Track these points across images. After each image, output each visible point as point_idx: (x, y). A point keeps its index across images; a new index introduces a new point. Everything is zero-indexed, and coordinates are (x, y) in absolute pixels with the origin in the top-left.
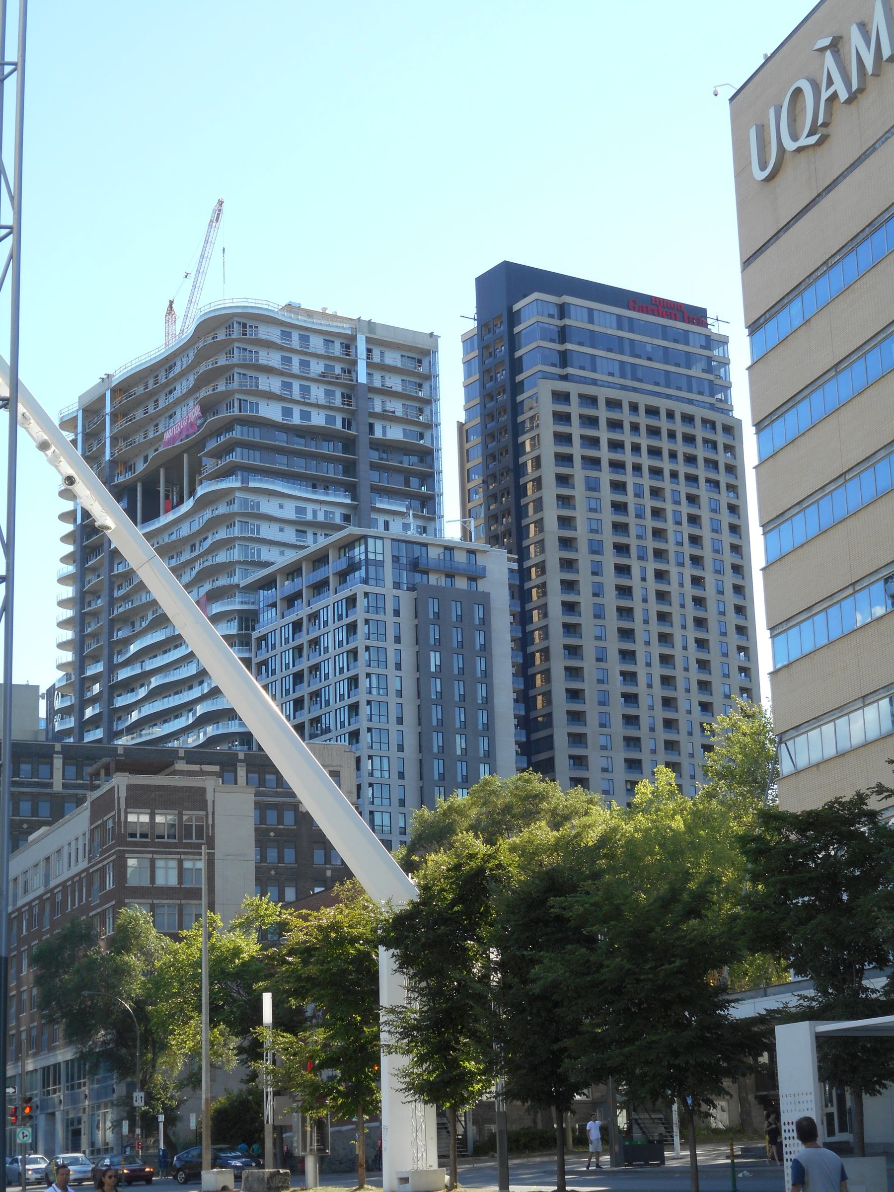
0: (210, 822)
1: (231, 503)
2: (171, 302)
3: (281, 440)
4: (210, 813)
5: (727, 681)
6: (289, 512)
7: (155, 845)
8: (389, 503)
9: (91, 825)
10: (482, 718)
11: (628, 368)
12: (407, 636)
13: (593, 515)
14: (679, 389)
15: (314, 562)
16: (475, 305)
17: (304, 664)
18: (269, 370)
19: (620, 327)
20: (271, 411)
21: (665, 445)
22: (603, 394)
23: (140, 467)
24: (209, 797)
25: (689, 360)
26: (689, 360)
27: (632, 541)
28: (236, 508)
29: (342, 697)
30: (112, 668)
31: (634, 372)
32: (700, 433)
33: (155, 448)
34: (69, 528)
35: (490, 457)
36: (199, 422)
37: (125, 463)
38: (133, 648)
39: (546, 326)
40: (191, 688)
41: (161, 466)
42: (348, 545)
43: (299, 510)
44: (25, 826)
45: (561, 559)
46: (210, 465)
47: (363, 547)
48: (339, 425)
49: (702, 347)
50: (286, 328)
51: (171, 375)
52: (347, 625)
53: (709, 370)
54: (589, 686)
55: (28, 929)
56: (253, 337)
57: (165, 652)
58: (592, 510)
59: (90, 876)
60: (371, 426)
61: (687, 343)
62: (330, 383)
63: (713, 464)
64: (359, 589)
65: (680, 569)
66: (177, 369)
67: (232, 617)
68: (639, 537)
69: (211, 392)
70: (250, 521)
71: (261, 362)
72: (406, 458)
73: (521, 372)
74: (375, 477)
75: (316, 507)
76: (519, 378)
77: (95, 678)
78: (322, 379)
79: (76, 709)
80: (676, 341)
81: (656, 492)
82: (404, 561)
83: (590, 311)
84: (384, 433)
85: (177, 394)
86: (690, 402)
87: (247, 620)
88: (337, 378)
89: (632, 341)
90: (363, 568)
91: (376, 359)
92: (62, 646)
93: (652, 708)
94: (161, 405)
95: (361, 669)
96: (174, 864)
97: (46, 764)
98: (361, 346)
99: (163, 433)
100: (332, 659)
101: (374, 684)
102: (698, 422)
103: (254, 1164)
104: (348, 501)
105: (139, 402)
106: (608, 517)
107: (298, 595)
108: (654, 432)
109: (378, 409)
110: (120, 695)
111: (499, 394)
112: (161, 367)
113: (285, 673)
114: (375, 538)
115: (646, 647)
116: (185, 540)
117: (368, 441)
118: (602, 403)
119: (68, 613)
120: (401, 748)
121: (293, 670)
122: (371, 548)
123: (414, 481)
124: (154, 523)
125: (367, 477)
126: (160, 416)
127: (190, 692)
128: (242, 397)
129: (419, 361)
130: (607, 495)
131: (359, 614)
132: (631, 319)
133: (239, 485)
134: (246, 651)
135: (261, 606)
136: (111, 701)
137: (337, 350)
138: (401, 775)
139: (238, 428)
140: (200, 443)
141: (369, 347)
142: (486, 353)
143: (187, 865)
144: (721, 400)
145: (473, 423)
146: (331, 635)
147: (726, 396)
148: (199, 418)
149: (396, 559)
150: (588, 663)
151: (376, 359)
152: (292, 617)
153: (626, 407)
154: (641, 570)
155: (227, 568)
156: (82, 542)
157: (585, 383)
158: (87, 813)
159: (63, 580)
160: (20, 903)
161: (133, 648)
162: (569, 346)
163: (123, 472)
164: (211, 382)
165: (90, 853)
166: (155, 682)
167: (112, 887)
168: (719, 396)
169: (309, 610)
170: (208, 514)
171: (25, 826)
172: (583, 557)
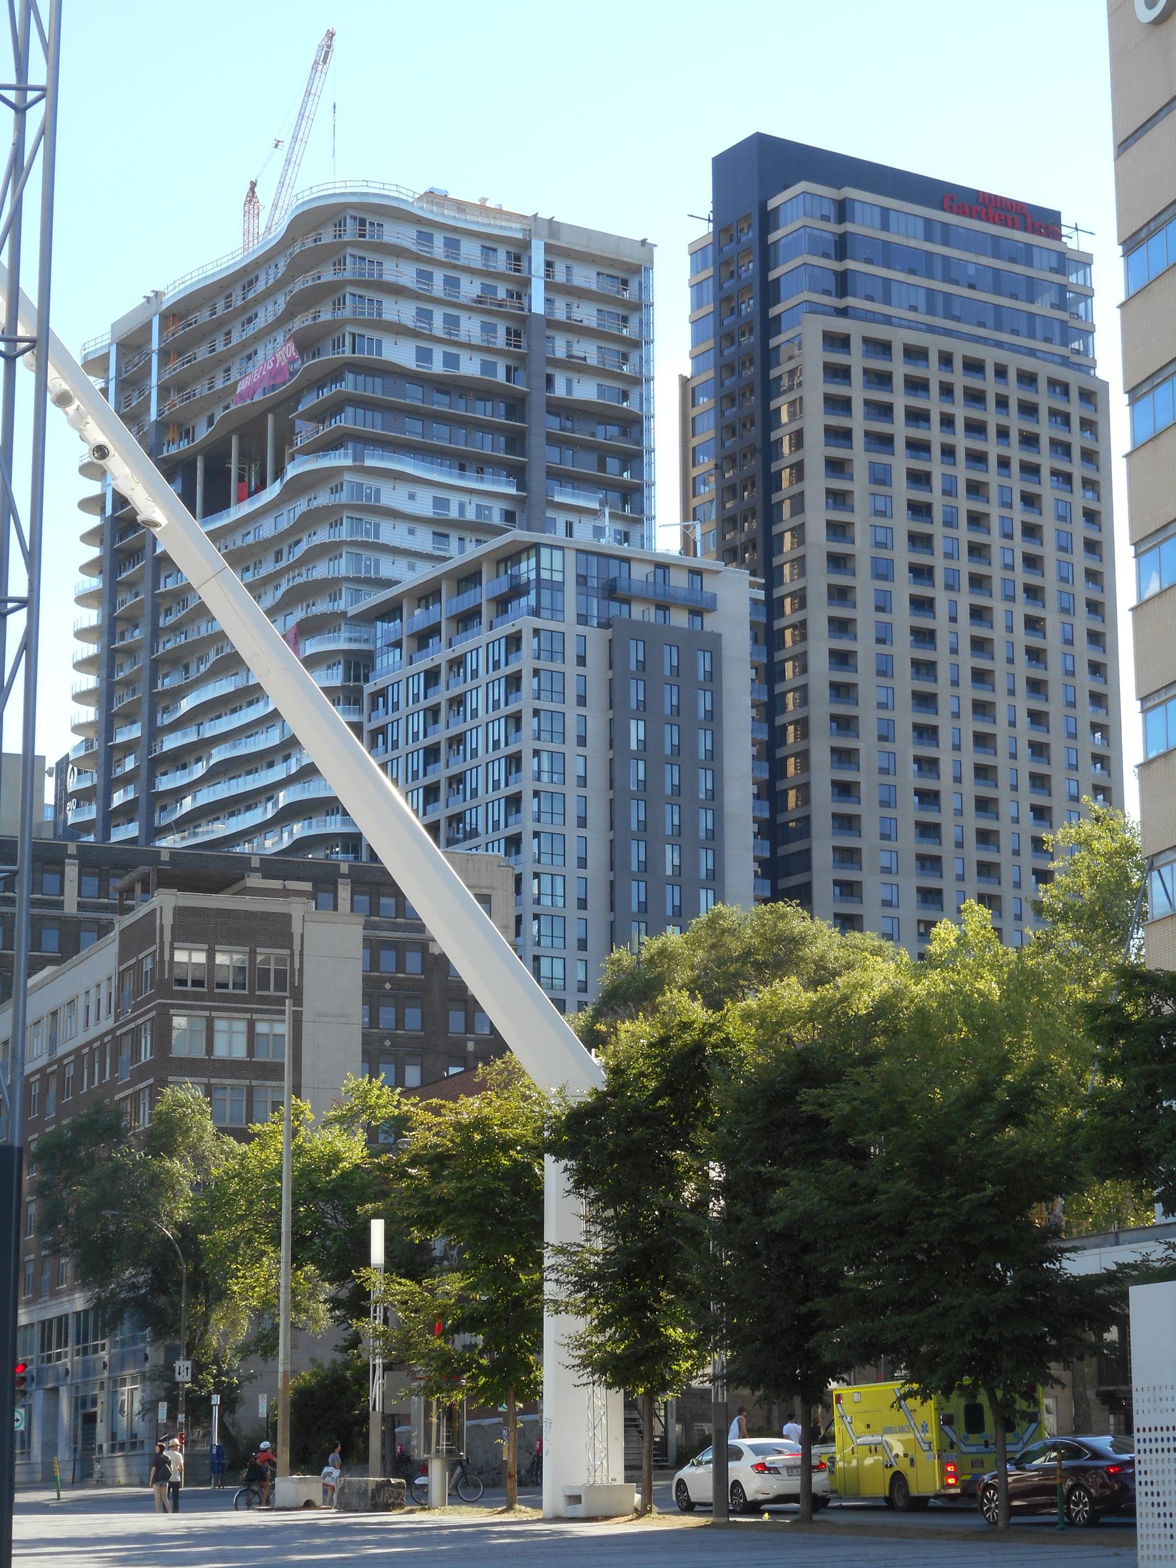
0: (297, 966)
2: (253, 185)
3: (414, 396)
4: (297, 952)
5: (1073, 774)
6: (423, 505)
7: (212, 997)
8: (573, 495)
11: (940, 300)
12: (597, 695)
13: (879, 521)
14: (1015, 332)
15: (459, 582)
16: (710, 198)
17: (441, 734)
18: (397, 291)
19: (928, 238)
21: (991, 417)
22: (900, 338)
23: (202, 433)
24: (296, 929)
25: (1031, 289)
26: (1031, 289)
28: (344, 497)
30: (154, 733)
32: (1044, 400)
35: (727, 429)
37: (180, 426)
38: (186, 705)
40: (271, 765)
43: (440, 503)
45: (830, 586)
46: (306, 433)
48: (501, 377)
49: (1052, 270)
50: (425, 227)
51: (251, 295)
54: (866, 777)
57: (234, 711)
58: (878, 513)
61: (1029, 263)
62: (489, 313)
63: (1062, 448)
65: (1009, 605)
66: (261, 287)
72: (600, 429)
73: (777, 301)
74: (553, 455)
75: (465, 498)
77: (128, 748)
78: (478, 306)
80: (1013, 260)
81: (975, 489)
82: (594, 583)
83: (885, 211)
84: (569, 390)
85: (260, 323)
86: (1032, 353)
87: (357, 665)
88: (500, 306)
89: (946, 259)
90: (533, 592)
91: (560, 277)
93: (959, 812)
94: (236, 339)
95: (525, 743)
96: (241, 1026)
98: (538, 257)
99: (237, 383)
100: (484, 726)
101: (545, 766)
102: (1042, 383)
104: (512, 491)
105: (204, 334)
108: (975, 397)
109: (560, 353)
110: (165, 774)
112: (236, 282)
113: (412, 746)
115: (955, 724)
118: (898, 351)
119: (90, 649)
120: (583, 863)
121: (423, 742)
122: (545, 563)
123: (613, 464)
124: (221, 518)
125: (541, 455)
126: (233, 356)
127: (271, 771)
129: (625, 283)
130: (901, 490)
131: (525, 661)
132: (945, 225)
133: (349, 462)
135: (379, 645)
136: (151, 783)
137: (501, 263)
138: (583, 904)
139: (350, 377)
140: (295, 397)
141: (550, 259)
142: (725, 273)
143: (261, 1028)
144: (1078, 352)
147: (1086, 346)
149: (582, 580)
150: (866, 743)
153: (934, 358)
154: (951, 605)
155: (330, 587)
156: (112, 545)
157: (874, 321)
161: (186, 705)
162: (850, 264)
163: (177, 440)
165: (117, 1006)
166: (219, 754)
167: (149, 1057)
168: (1075, 345)
170: (302, 506)
172: (863, 584)
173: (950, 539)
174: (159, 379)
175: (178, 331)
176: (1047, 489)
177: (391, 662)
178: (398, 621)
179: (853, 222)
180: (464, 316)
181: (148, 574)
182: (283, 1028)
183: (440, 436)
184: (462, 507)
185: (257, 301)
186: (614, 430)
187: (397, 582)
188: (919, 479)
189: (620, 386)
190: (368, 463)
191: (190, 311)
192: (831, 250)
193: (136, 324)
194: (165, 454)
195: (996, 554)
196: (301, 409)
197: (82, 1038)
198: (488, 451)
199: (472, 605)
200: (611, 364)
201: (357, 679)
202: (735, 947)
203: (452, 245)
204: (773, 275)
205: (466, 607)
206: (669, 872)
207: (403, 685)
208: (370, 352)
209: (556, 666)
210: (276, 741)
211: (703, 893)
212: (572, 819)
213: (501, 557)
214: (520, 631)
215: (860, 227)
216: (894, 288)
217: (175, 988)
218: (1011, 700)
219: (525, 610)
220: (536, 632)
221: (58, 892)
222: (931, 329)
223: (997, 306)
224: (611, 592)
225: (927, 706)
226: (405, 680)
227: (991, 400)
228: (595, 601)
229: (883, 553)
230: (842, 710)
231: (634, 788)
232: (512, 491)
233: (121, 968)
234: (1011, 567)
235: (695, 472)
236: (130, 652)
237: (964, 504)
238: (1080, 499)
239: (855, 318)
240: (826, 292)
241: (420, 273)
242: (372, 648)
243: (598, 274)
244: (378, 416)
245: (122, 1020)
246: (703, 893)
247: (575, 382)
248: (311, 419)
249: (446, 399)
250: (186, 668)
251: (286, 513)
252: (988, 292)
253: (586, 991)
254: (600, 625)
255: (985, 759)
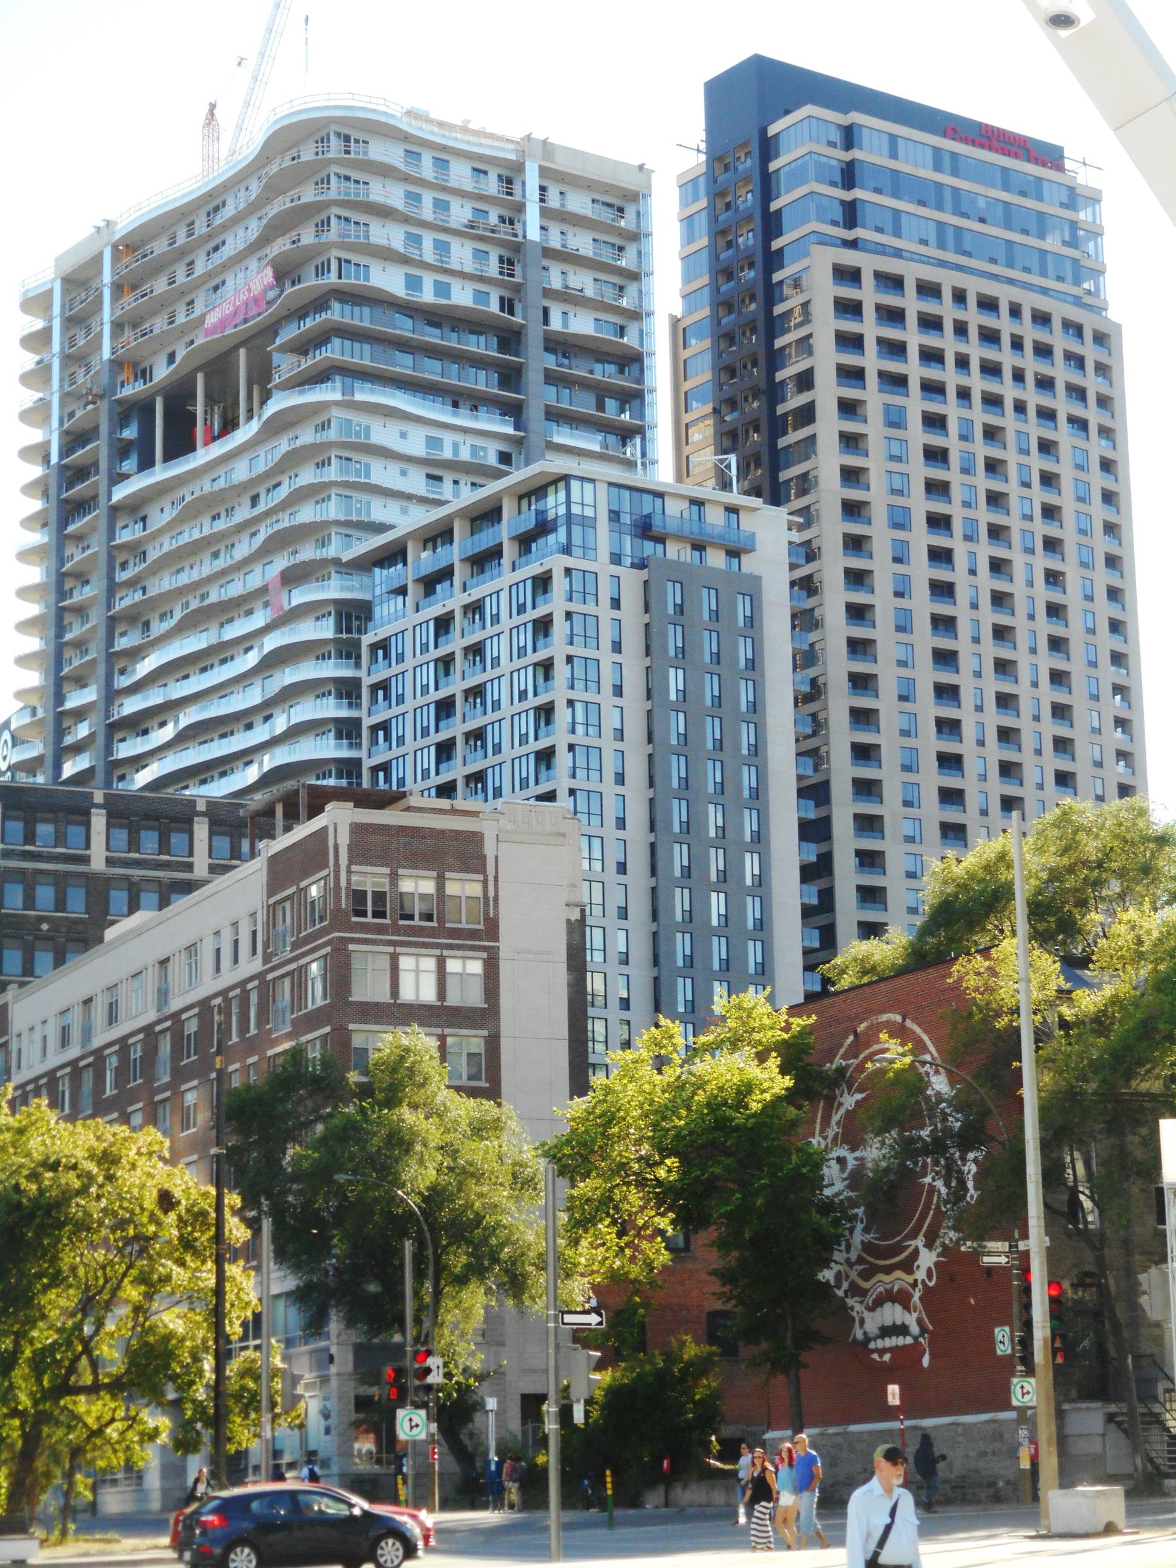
0: (491, 894)
1: (324, 426)
2: (213, 107)
3: (404, 327)
4: (491, 878)
5: (1097, 739)
6: (415, 443)
7: (397, 931)
8: (572, 436)
9: (269, 896)
10: (748, 778)
11: (950, 234)
12: (633, 641)
13: (895, 466)
14: (1027, 270)
15: (473, 520)
16: (703, 126)
17: (456, 686)
18: (384, 212)
19: (938, 168)
20: (388, 280)
21: (1007, 358)
22: (912, 272)
23: (161, 372)
24: (489, 850)
25: (1042, 225)
26: (1042, 225)
27: (954, 509)
28: (332, 435)
29: (524, 740)
30: (111, 695)
31: (957, 240)
32: (1060, 342)
33: (188, 339)
34: (36, 471)
35: (727, 370)
36: (271, 295)
37: (135, 365)
38: (145, 667)
39: (824, 159)
40: (249, 727)
41: (198, 369)
42: (537, 491)
43: (432, 442)
44: (45, 927)
45: (845, 535)
46: (286, 365)
47: (562, 495)
48: (494, 307)
49: (1062, 205)
50: (413, 145)
51: (218, 221)
52: (535, 621)
53: (1073, 243)
54: (886, 738)
55: (117, 1084)
56: (361, 157)
57: (204, 670)
58: (893, 458)
59: (267, 988)
60: (546, 311)
61: (1040, 197)
62: (481, 239)
63: (1078, 393)
64: (557, 563)
65: (1029, 558)
66: (229, 212)
67: (325, 611)
68: (966, 504)
69: (288, 246)
70: (355, 456)
71: (373, 198)
72: (598, 367)
73: (779, 234)
74: (550, 395)
75: (458, 437)
76: (776, 245)
77: (79, 714)
78: (470, 232)
79: (49, 762)
80: (1023, 194)
81: (992, 433)
82: (626, 519)
83: (893, 138)
84: (565, 323)
85: (228, 251)
86: (1044, 291)
87: (349, 617)
88: (493, 231)
89: (956, 190)
90: (562, 531)
91: (554, 201)
92: (23, 661)
93: (984, 778)
94: (200, 269)
95: (558, 691)
96: (429, 964)
97: (77, 823)
98: (532, 180)
99: (203, 316)
100: (507, 675)
101: (580, 717)
102: (1057, 323)
103: (1001, 1484)
104: (509, 430)
105: (158, 267)
106: (919, 470)
107: (446, 573)
108: (990, 337)
109: (556, 283)
110: (123, 740)
111: (742, 270)
112: (199, 207)
113: (420, 701)
114: (583, 479)
115: (977, 684)
116: (239, 489)
117: (542, 334)
118: (910, 286)
119: (33, 609)
120: (621, 823)
121: (434, 696)
122: (575, 496)
123: (611, 404)
124: (188, 461)
125: (539, 395)
126: (197, 287)
127: (250, 733)
128: (344, 255)
129: (621, 210)
130: (917, 436)
131: (556, 604)
132: (954, 156)
133: (337, 396)
134: (348, 667)
135: (378, 592)
136: (109, 750)
137: (492, 186)
138: (622, 868)
139: (336, 306)
140: (272, 329)
141: (544, 184)
142: (720, 205)
143: (453, 966)
144: (1089, 292)
145: (696, 317)
146: (504, 639)
147: (1097, 287)
148: (272, 288)
149: (615, 516)
150: (885, 703)
151: (554, 201)
152: (436, 609)
153: (947, 294)
154: (971, 554)
155: (316, 531)
156: (59, 494)
157: (883, 254)
158: (263, 877)
159: (25, 555)
160: (97, 1042)
161: (145, 667)
162: (858, 193)
163: (132, 379)
164: (290, 230)
165: (266, 945)
166: (189, 717)
167: (320, 1002)
168: (1086, 285)
169: (466, 599)
170: (283, 445)
171: (45, 927)
172: (879, 532)
173: (967, 487)
174: (112, 314)
175: (132, 263)
176: (1063, 435)
177: (392, 610)
178: (400, 566)
179: (861, 148)
180: (456, 244)
181: (103, 524)
182: (475, 967)
183: (432, 370)
184: (456, 447)
185: (224, 227)
186: (611, 368)
187: (392, 527)
188: (935, 422)
189: (618, 320)
190: (359, 397)
191: (144, 242)
192: (838, 178)
193: (86, 255)
194: (119, 396)
195: (1014, 503)
196: (278, 341)
197: (208, 986)
198: (482, 387)
199: (491, 544)
200: (609, 296)
201: (349, 631)
202: (1091, 848)
203: (441, 164)
204: (774, 206)
205: (484, 547)
206: (712, 834)
207: (408, 636)
208: (357, 278)
209: (589, 608)
210: (257, 700)
211: (748, 856)
212: (609, 776)
213: (524, 491)
214: (550, 571)
215: (868, 154)
216: (904, 219)
217: (354, 919)
218: (1033, 659)
219: (555, 547)
220: (568, 571)
221: (83, 845)
222: (942, 264)
223: (1009, 243)
224: (645, 530)
225: (946, 664)
226: (410, 631)
227: (1006, 341)
228: (628, 538)
229: (899, 501)
230: (861, 667)
231: (674, 742)
232: (509, 430)
233: (272, 901)
234: (1030, 518)
235: (687, 418)
236: (80, 611)
237: (982, 450)
238: (1097, 447)
239: (865, 250)
240: (834, 223)
241: (409, 195)
242: (368, 597)
243: (593, 201)
244: (367, 347)
245: (275, 961)
246: (748, 856)
247: (571, 315)
248: (293, 350)
249: (437, 332)
250: (147, 625)
251: (262, 454)
252: (998, 226)
253: (627, 963)
254: (633, 566)
255: (1008, 721)
